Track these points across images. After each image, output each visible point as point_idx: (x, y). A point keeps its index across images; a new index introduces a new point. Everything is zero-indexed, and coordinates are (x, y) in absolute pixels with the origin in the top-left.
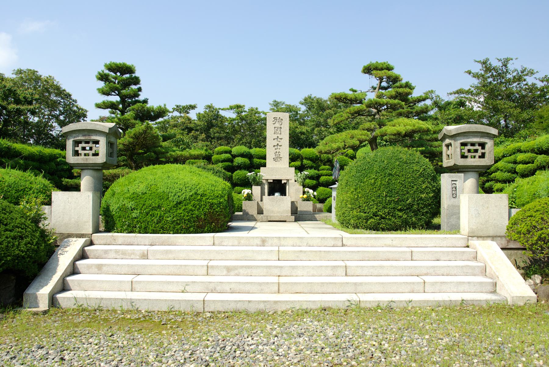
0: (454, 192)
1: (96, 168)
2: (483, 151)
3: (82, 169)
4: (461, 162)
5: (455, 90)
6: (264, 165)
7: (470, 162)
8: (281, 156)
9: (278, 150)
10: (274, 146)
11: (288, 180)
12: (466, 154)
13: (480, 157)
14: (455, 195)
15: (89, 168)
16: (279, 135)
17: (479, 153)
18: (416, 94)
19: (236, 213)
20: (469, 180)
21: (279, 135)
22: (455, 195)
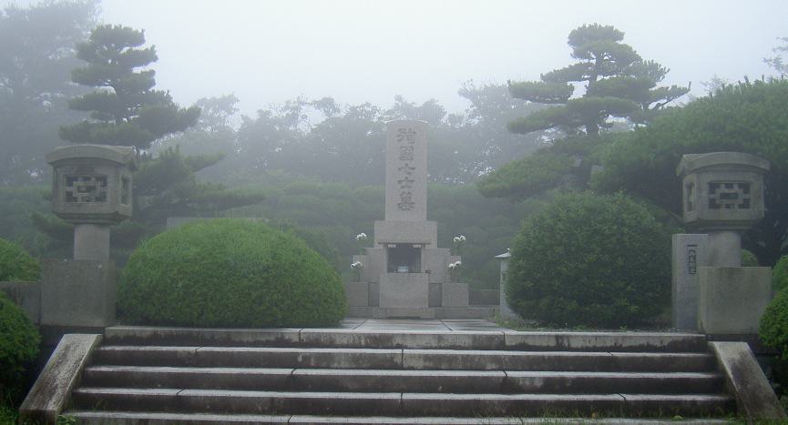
0: (691, 265)
1: (101, 221)
2: (747, 196)
3: (76, 224)
4: (709, 215)
5: (319, 98)
6: (382, 218)
7: (725, 214)
8: (412, 200)
9: (406, 190)
10: (400, 182)
11: (423, 244)
12: (718, 202)
13: (741, 206)
14: (693, 270)
15: (90, 221)
16: (408, 162)
17: (740, 201)
18: (665, 83)
19: (611, 119)
20: (748, 347)
21: (408, 162)
22: (693, 270)
